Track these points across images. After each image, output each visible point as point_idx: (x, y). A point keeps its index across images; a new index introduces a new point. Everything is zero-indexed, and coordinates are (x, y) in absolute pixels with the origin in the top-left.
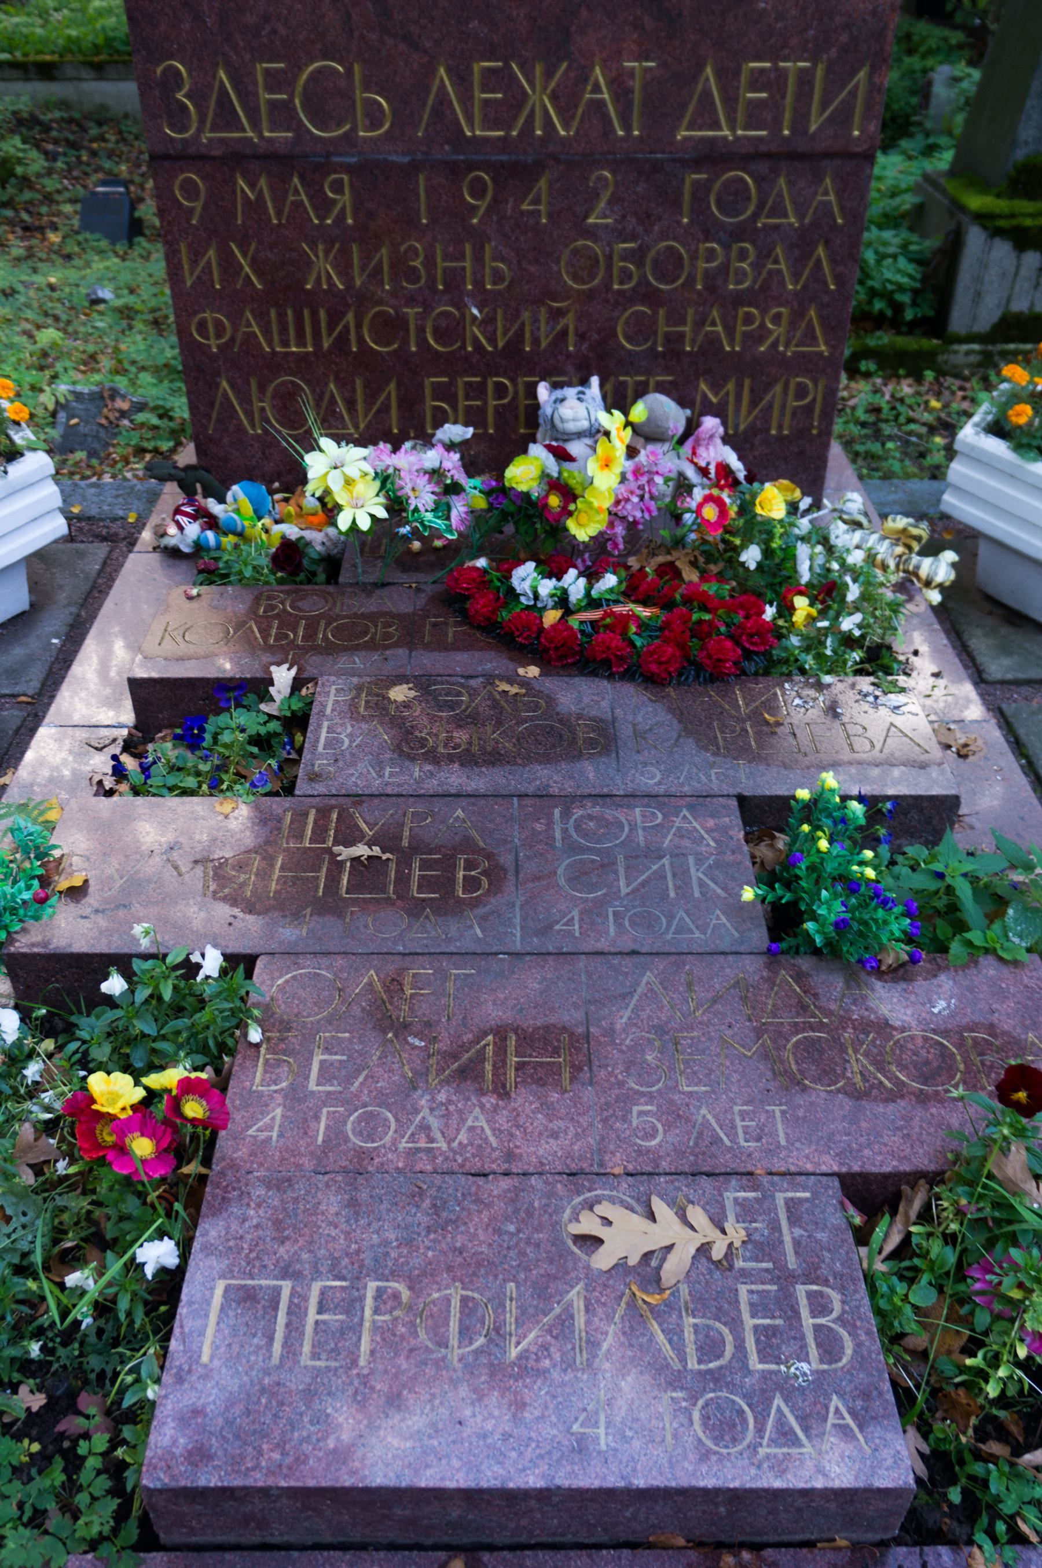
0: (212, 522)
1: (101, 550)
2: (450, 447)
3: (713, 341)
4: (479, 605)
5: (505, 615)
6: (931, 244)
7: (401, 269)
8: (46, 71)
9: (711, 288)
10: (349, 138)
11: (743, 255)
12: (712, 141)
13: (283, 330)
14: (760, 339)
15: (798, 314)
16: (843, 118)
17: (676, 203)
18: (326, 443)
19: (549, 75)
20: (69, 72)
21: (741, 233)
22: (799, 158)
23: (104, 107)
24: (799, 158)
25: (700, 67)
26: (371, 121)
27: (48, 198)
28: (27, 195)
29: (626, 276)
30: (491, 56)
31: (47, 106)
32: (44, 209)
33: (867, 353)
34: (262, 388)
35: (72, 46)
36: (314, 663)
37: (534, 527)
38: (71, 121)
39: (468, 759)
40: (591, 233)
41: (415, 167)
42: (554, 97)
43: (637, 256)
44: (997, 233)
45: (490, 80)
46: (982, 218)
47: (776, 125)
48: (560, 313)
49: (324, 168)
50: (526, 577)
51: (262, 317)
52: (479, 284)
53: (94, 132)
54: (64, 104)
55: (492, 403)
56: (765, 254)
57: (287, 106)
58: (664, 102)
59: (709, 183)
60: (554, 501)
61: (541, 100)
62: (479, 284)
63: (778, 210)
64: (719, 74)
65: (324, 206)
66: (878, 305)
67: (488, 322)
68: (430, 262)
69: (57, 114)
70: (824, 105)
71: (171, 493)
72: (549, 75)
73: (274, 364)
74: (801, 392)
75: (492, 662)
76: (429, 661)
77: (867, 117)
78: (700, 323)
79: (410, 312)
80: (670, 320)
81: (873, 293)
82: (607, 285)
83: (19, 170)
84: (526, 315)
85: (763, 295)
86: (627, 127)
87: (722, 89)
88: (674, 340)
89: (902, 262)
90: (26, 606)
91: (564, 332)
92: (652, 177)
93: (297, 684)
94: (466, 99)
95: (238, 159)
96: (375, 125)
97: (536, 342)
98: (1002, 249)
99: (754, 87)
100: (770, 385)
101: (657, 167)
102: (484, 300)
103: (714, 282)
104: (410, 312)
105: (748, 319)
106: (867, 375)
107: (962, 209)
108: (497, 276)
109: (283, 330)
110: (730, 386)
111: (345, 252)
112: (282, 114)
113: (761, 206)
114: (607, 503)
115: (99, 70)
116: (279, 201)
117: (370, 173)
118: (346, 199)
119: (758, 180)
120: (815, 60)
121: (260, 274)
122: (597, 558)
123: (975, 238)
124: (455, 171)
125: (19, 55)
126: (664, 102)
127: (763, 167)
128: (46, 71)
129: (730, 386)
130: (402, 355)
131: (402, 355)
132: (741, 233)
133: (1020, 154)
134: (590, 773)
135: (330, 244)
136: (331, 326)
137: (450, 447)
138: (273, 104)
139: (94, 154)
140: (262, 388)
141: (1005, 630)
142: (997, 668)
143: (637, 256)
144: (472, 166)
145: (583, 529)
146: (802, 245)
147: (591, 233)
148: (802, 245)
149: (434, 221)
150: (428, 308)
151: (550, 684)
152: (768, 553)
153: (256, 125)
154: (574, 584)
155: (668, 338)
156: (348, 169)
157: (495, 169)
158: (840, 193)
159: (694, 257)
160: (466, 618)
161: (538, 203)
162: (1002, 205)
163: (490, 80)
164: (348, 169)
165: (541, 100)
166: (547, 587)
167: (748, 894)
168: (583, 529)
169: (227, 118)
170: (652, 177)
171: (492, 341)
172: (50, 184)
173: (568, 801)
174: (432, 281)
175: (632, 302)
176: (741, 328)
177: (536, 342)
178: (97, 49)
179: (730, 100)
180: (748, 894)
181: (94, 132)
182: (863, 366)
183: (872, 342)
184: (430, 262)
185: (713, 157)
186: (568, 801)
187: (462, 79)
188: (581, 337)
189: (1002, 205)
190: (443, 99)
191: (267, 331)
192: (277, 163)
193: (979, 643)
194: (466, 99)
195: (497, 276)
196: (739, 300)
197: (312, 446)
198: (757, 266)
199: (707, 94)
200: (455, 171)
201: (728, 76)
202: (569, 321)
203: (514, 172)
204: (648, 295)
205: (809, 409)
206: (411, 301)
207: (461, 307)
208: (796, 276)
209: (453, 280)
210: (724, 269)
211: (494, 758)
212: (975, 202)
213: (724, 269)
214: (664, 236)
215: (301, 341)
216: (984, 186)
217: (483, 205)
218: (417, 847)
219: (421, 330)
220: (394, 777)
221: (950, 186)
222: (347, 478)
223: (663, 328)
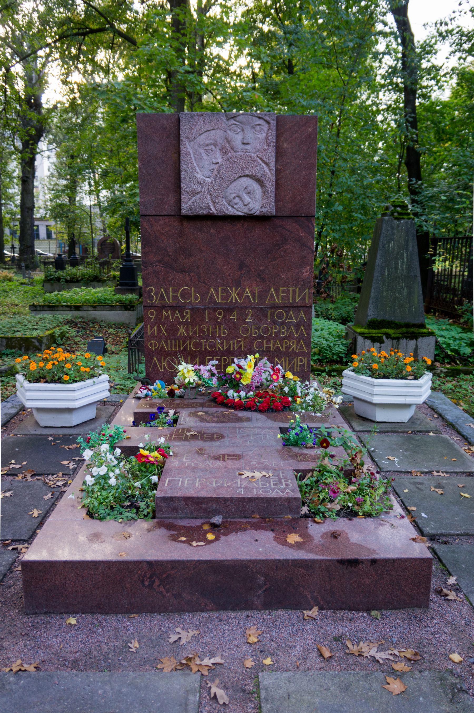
0: (150, 390)
1: (114, 408)
2: (213, 366)
3: (278, 348)
4: (220, 399)
5: (225, 401)
6: (349, 342)
7: (201, 331)
8: (77, 308)
9: (276, 336)
10: (190, 303)
11: (283, 328)
12: (274, 304)
13: (171, 345)
14: (289, 348)
15: (298, 342)
16: (304, 299)
17: (267, 316)
18: (183, 363)
19: (236, 290)
20: (85, 308)
21: (282, 324)
22: (295, 307)
23: (95, 318)
24: (295, 307)
25: (270, 288)
26: (195, 299)
27: (76, 343)
28: (69, 342)
29: (255, 333)
30: (223, 286)
31: (77, 318)
32: (74, 346)
33: (334, 370)
34: (164, 359)
35: (87, 301)
36: (179, 410)
37: (234, 382)
38: (84, 322)
39: (216, 422)
40: (247, 323)
41: (205, 309)
42: (237, 294)
43: (258, 328)
44: (366, 338)
45: (223, 291)
46: (361, 334)
47: (289, 300)
48: (240, 341)
49: (184, 309)
50: (231, 393)
51: (166, 342)
52: (220, 334)
53: (91, 325)
54: (82, 317)
55: (223, 363)
56: (289, 328)
57: (176, 296)
58: (263, 295)
59: (274, 313)
60: (238, 376)
61: (234, 295)
62: (220, 334)
63: (291, 318)
64: (275, 290)
65: (183, 317)
66: (335, 357)
67: (222, 343)
68: (208, 330)
69: (80, 320)
70: (299, 296)
71: (139, 384)
72: (236, 290)
73: (168, 354)
74: (301, 361)
75: (222, 409)
76: (206, 409)
77: (309, 299)
78: (274, 345)
79: (203, 341)
80: (267, 343)
81: (333, 354)
82: (251, 335)
83: (67, 335)
84: (231, 342)
85: (289, 337)
86: (254, 300)
87: (276, 293)
88: (268, 348)
89: (341, 346)
90: (94, 416)
91: (241, 346)
92: (261, 311)
93: (175, 413)
94: (217, 295)
95: (164, 307)
96: (196, 300)
97: (234, 348)
98: (368, 342)
99: (282, 292)
100: (293, 359)
101: (262, 309)
102: (221, 338)
103: (277, 334)
104: (203, 341)
105: (286, 343)
106: (334, 376)
107: (356, 332)
108: (224, 333)
109: (171, 345)
110: (283, 359)
111: (188, 327)
112: (175, 298)
113: (287, 317)
114: (251, 377)
115: (95, 308)
116: (173, 316)
117: (195, 311)
118: (189, 316)
119: (286, 312)
120: (296, 287)
121: (167, 332)
122: (248, 388)
123: (360, 339)
124: (215, 310)
125: (69, 304)
126: (263, 295)
127: (286, 309)
128: (77, 308)
129: (283, 359)
130: (200, 351)
131: (200, 351)
132: (282, 324)
133: (369, 318)
134: (245, 424)
135: (184, 325)
136: (183, 344)
137: (213, 366)
138: (173, 296)
139: (91, 331)
140: (164, 359)
141: (362, 422)
142: (358, 428)
143: (258, 328)
144: (218, 309)
145: (245, 382)
146: (297, 326)
147: (247, 323)
148: (297, 326)
149: (209, 320)
150: (207, 340)
151: (236, 412)
152: (289, 387)
153: (169, 300)
154: (243, 394)
155: (267, 347)
156: (189, 309)
157: (225, 310)
158: (305, 315)
159: (272, 329)
160: (216, 402)
161: (234, 316)
162: (366, 331)
163: (223, 291)
164: (189, 309)
165: (234, 295)
166: (235, 395)
167: (279, 436)
168: (245, 382)
169: (162, 298)
170: (261, 311)
171: (223, 348)
172: (77, 339)
173: (240, 428)
174: (208, 333)
175: (257, 339)
176: (284, 345)
177: (234, 348)
178: (95, 302)
179: (278, 295)
180: (279, 436)
181: (91, 325)
182: (333, 374)
183: (334, 367)
184: (208, 330)
185: (274, 307)
186: (240, 428)
187: (216, 291)
188: (245, 347)
189: (366, 331)
190: (212, 295)
191: (167, 346)
192: (173, 308)
193: (355, 424)
194: (217, 295)
195: (224, 333)
196: (284, 338)
197: (179, 363)
198: (287, 331)
199: (272, 294)
200: (215, 310)
201: (277, 290)
202: (242, 343)
203: (229, 310)
204: (261, 337)
205: (304, 365)
206: (203, 338)
207: (215, 340)
208: (297, 333)
209: (214, 333)
210: (279, 331)
211: (223, 422)
212: (359, 330)
213: (279, 331)
214: (264, 324)
215: (175, 348)
216: (362, 327)
217: (221, 317)
218: (204, 434)
219: (205, 345)
220: (199, 424)
221: (353, 328)
222: (187, 372)
223: (265, 345)
